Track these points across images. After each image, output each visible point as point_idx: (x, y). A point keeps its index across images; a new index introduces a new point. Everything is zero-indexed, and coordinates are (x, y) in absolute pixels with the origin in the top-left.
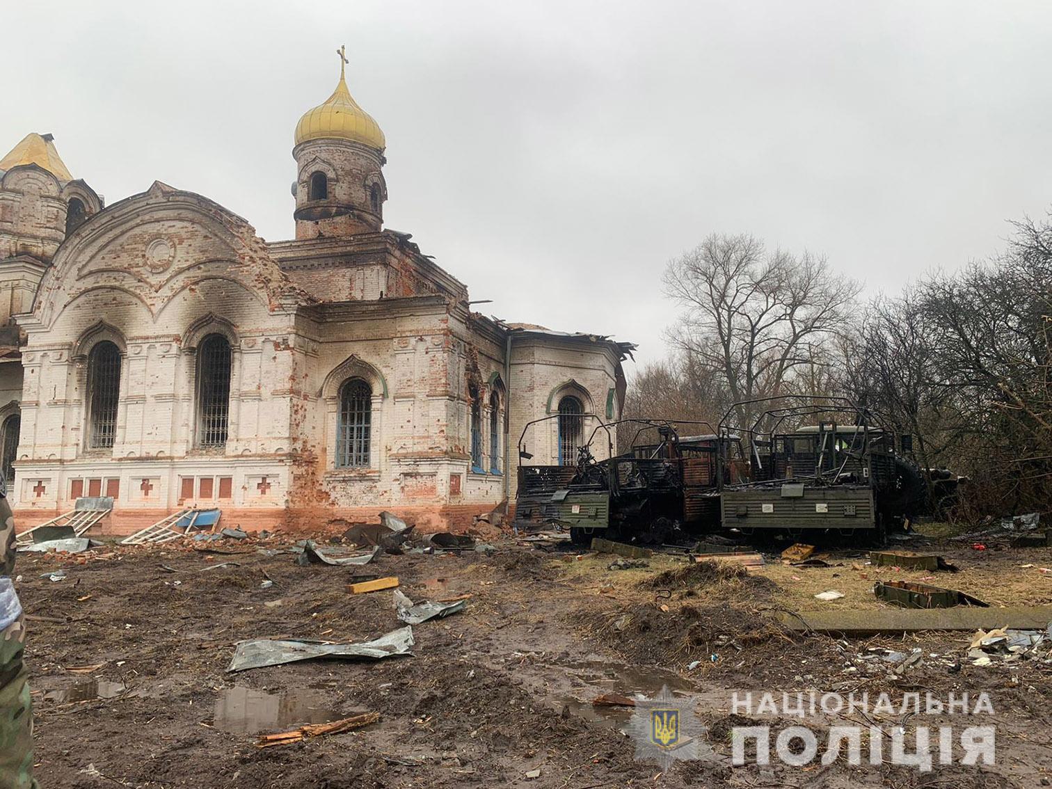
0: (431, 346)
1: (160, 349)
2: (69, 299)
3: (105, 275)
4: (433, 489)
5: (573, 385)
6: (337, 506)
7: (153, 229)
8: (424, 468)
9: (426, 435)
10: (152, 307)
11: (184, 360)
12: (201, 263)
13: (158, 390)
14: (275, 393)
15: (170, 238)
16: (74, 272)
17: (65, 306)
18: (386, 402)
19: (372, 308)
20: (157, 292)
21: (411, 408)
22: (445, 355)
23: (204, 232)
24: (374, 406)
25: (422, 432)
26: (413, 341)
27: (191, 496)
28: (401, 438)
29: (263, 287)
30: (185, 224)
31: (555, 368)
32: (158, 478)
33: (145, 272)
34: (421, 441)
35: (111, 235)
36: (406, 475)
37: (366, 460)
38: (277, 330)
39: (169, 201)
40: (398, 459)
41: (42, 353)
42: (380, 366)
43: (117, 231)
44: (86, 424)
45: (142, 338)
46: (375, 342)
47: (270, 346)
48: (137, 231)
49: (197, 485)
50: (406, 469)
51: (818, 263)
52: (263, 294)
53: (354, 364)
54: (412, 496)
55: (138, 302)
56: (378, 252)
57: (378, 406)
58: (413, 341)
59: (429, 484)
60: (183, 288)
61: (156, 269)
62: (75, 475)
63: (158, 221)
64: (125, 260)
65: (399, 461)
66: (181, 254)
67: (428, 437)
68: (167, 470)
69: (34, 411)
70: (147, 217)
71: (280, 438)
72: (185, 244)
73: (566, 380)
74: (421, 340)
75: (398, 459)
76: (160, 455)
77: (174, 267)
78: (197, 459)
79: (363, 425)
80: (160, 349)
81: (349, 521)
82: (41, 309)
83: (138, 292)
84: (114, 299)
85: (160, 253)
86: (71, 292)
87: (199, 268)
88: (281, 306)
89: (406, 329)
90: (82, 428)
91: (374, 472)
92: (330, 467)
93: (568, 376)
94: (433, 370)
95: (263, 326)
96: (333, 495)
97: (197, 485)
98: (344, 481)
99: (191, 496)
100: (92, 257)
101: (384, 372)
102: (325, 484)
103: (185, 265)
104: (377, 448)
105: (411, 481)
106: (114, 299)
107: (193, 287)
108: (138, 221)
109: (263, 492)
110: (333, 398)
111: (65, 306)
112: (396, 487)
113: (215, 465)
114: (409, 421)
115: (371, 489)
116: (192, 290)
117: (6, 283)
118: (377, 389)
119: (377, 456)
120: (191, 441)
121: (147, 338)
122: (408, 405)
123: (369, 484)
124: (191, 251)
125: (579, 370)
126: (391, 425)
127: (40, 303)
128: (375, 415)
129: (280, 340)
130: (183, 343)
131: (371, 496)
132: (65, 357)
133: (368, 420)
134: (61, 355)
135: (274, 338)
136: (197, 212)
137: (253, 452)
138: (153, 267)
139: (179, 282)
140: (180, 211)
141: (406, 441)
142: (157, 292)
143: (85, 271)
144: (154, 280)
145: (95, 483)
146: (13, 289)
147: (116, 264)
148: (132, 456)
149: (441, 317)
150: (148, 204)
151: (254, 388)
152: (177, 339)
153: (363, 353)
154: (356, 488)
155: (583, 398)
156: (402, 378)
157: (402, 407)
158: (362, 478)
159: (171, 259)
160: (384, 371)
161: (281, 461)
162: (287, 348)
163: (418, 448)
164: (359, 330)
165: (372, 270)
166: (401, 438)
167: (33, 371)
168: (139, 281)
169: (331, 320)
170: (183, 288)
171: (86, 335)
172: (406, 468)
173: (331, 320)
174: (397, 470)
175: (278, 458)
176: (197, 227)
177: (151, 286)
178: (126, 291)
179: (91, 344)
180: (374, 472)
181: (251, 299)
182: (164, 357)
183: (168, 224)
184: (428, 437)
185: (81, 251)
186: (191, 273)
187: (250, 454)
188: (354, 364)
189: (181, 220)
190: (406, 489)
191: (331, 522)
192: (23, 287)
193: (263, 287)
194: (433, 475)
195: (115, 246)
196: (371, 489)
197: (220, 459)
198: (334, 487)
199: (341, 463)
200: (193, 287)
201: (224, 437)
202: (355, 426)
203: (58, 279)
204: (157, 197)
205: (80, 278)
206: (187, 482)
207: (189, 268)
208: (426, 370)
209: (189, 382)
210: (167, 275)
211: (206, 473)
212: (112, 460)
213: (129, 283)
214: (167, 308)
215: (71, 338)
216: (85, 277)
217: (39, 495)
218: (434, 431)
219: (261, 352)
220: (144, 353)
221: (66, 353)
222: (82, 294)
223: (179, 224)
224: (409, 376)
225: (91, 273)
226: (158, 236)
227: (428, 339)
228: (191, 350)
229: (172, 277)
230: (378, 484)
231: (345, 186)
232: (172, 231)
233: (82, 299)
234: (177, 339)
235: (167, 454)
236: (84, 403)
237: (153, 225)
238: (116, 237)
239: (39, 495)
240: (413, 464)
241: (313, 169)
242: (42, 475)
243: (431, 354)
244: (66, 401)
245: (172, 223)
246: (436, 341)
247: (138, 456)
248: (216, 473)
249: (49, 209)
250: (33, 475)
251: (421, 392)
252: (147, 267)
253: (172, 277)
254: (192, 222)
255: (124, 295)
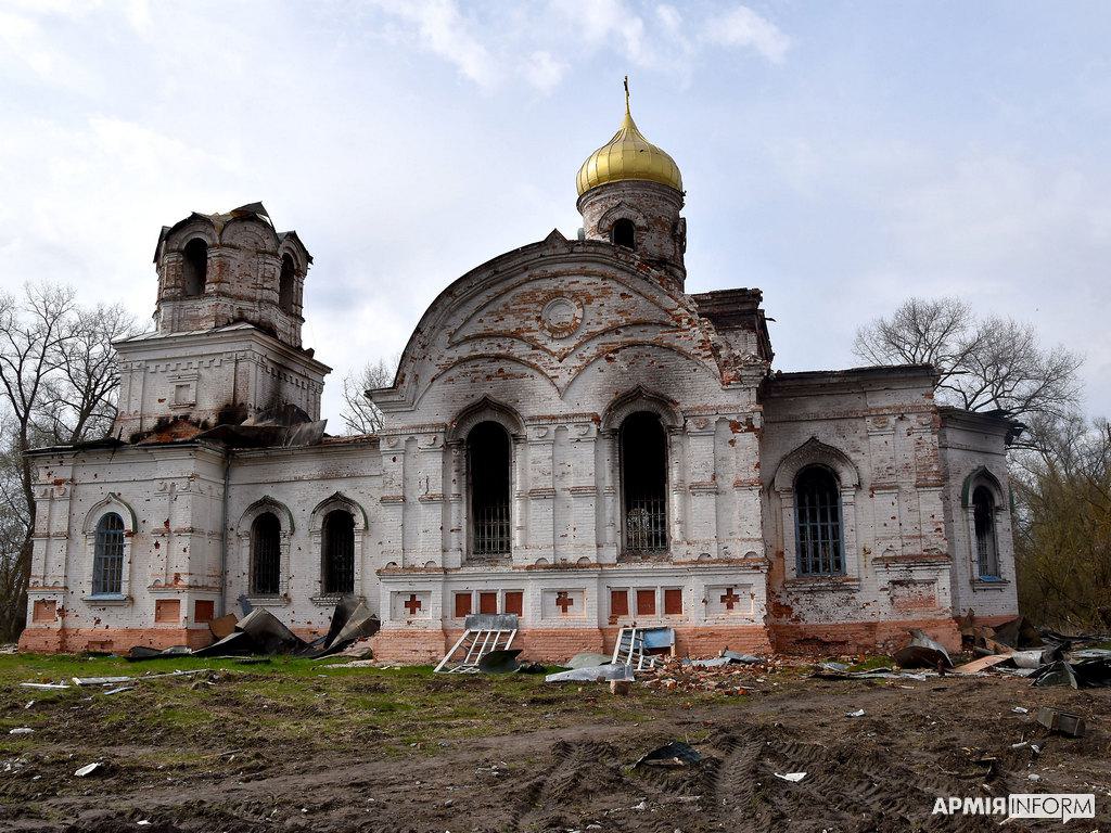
0: (917, 426)
1: (573, 432)
2: (437, 371)
3: (486, 342)
4: (931, 599)
5: (266, 501)
6: (802, 623)
7: (549, 285)
8: (920, 574)
9: (917, 533)
10: (555, 380)
11: (606, 448)
12: (622, 327)
13: (571, 482)
14: (738, 485)
15: (575, 296)
16: (443, 338)
17: (433, 380)
18: (861, 493)
19: (835, 380)
20: (560, 361)
21: (895, 501)
22: (936, 437)
23: (621, 289)
24: (845, 499)
25: (910, 531)
26: (892, 420)
27: (625, 612)
28: (885, 539)
29: (709, 356)
30: (593, 280)
31: (964, 453)
32: (582, 591)
33: (541, 338)
34: (912, 541)
35: (491, 292)
36: (895, 583)
37: (838, 564)
38: (736, 407)
39: (572, 252)
40: (886, 562)
41: (407, 438)
42: (846, 451)
43: (499, 288)
44: (468, 523)
45: (545, 417)
46: (837, 421)
47: (726, 427)
48: (527, 288)
49: (632, 599)
50: (895, 576)
51: (1023, 333)
52: (712, 364)
53: (814, 449)
54: (905, 608)
55: (536, 374)
56: (743, 313)
57: (851, 499)
58: (892, 420)
59: (926, 594)
60: (598, 357)
61: (557, 332)
62: (462, 587)
63: (555, 276)
64: (511, 323)
65: (887, 566)
66: (591, 316)
67: (920, 537)
68: (592, 581)
69: (400, 509)
70: (537, 272)
71: (749, 540)
72: (595, 304)
73: (327, 495)
74: (901, 419)
75: (886, 562)
76: (583, 562)
77: (584, 331)
78: (472, 570)
79: (117, 544)
80: (573, 432)
81: (826, 640)
82: (406, 384)
83: (533, 361)
84: (501, 370)
85: (568, 313)
86: (440, 362)
87: (618, 333)
88: (739, 378)
89: (879, 405)
90: (464, 529)
91: (853, 580)
92: (792, 575)
93: (977, 461)
94: (920, 455)
95: (713, 403)
96: (796, 609)
97: (632, 599)
98: (811, 592)
99: (625, 612)
100: (468, 320)
101: (853, 458)
102: (784, 595)
103: (599, 328)
104: (854, 551)
105: (900, 591)
106: (501, 370)
107: (611, 355)
108: (526, 275)
109: (730, 607)
110: (788, 490)
111: (433, 380)
112: (884, 597)
113: (501, 577)
114: (894, 518)
115: (847, 602)
116: (609, 359)
117: (229, 355)
118: (847, 477)
119: (852, 562)
120: (465, 550)
121: (554, 418)
122: (892, 498)
123: (845, 595)
124: (604, 310)
125: (986, 456)
126: (867, 523)
127: (404, 376)
128: (847, 513)
129: (743, 420)
130: (602, 424)
131: (848, 610)
132: (440, 441)
133: (836, 515)
134: (435, 439)
135: (733, 418)
136: (611, 265)
137: (714, 556)
138: (553, 330)
139: (591, 350)
140: (584, 265)
141: (893, 542)
142: (560, 361)
143: (458, 338)
144: (555, 347)
145: (488, 599)
146: (237, 362)
147: (500, 327)
148: (543, 563)
149: (924, 391)
150: (542, 256)
151: (708, 478)
152: (596, 419)
153: (826, 434)
154: (827, 601)
155: (993, 489)
156: (880, 466)
157: (883, 501)
158: (837, 588)
159: (578, 321)
160: (853, 456)
161: (757, 568)
162: (751, 428)
163: (909, 550)
164: (814, 407)
165: (737, 335)
166: (885, 539)
167: (394, 460)
168: (534, 348)
169: (776, 395)
170: (598, 357)
171: (464, 415)
172: (896, 574)
173: (776, 395)
174: (884, 578)
175: (748, 564)
176: (610, 283)
177: (553, 355)
178: (517, 361)
179: (469, 426)
180: (853, 580)
181: (695, 370)
182: (578, 440)
183: (568, 280)
184: (920, 537)
185: (452, 313)
186: (608, 339)
187: (708, 559)
188: (814, 449)
189: (588, 274)
190: (896, 600)
191: (799, 642)
192: (249, 360)
193: (709, 356)
194: (930, 582)
195: (498, 305)
196: (847, 602)
197: (667, 566)
198: (797, 600)
199: (803, 568)
200: (611, 355)
201: (505, 547)
202: (819, 525)
203: (423, 347)
204: (554, 247)
205: (454, 345)
206: (619, 598)
207: (603, 333)
208: (910, 455)
209: (612, 471)
210: (572, 343)
211: (645, 584)
212: (514, 568)
213: (520, 350)
214: (578, 381)
215: (445, 419)
216: (458, 344)
217: (413, 612)
218: (927, 529)
219: (714, 434)
220: (552, 436)
221: (441, 438)
222: (456, 364)
223: (585, 280)
224: (889, 462)
225: (467, 339)
226: (558, 294)
227: (913, 417)
228: (613, 432)
229: (581, 344)
230: (857, 595)
231: (655, 236)
232: (575, 287)
233: (455, 372)
234: (596, 419)
235: (593, 560)
236: (465, 498)
237: (548, 281)
238: (499, 296)
239: (413, 612)
240: (906, 564)
241: (617, 216)
242: (418, 587)
243: (915, 437)
244: (596, 488)
245: (575, 279)
246: (925, 420)
247: (551, 563)
248: (659, 585)
249: (267, 266)
250: (721, 580)
251: (907, 482)
252: (545, 332)
253: (581, 344)
254: (604, 277)
255: (513, 365)
